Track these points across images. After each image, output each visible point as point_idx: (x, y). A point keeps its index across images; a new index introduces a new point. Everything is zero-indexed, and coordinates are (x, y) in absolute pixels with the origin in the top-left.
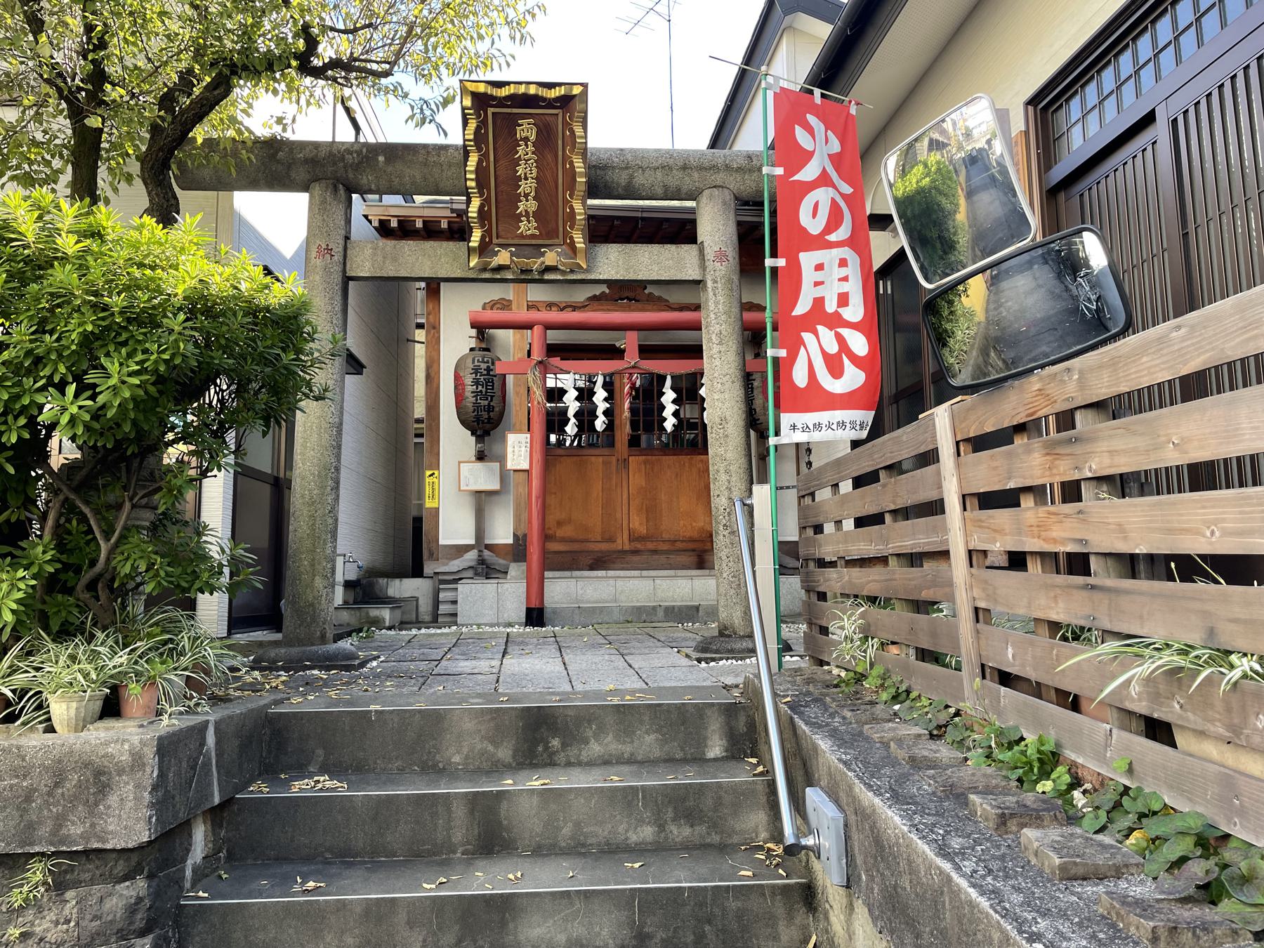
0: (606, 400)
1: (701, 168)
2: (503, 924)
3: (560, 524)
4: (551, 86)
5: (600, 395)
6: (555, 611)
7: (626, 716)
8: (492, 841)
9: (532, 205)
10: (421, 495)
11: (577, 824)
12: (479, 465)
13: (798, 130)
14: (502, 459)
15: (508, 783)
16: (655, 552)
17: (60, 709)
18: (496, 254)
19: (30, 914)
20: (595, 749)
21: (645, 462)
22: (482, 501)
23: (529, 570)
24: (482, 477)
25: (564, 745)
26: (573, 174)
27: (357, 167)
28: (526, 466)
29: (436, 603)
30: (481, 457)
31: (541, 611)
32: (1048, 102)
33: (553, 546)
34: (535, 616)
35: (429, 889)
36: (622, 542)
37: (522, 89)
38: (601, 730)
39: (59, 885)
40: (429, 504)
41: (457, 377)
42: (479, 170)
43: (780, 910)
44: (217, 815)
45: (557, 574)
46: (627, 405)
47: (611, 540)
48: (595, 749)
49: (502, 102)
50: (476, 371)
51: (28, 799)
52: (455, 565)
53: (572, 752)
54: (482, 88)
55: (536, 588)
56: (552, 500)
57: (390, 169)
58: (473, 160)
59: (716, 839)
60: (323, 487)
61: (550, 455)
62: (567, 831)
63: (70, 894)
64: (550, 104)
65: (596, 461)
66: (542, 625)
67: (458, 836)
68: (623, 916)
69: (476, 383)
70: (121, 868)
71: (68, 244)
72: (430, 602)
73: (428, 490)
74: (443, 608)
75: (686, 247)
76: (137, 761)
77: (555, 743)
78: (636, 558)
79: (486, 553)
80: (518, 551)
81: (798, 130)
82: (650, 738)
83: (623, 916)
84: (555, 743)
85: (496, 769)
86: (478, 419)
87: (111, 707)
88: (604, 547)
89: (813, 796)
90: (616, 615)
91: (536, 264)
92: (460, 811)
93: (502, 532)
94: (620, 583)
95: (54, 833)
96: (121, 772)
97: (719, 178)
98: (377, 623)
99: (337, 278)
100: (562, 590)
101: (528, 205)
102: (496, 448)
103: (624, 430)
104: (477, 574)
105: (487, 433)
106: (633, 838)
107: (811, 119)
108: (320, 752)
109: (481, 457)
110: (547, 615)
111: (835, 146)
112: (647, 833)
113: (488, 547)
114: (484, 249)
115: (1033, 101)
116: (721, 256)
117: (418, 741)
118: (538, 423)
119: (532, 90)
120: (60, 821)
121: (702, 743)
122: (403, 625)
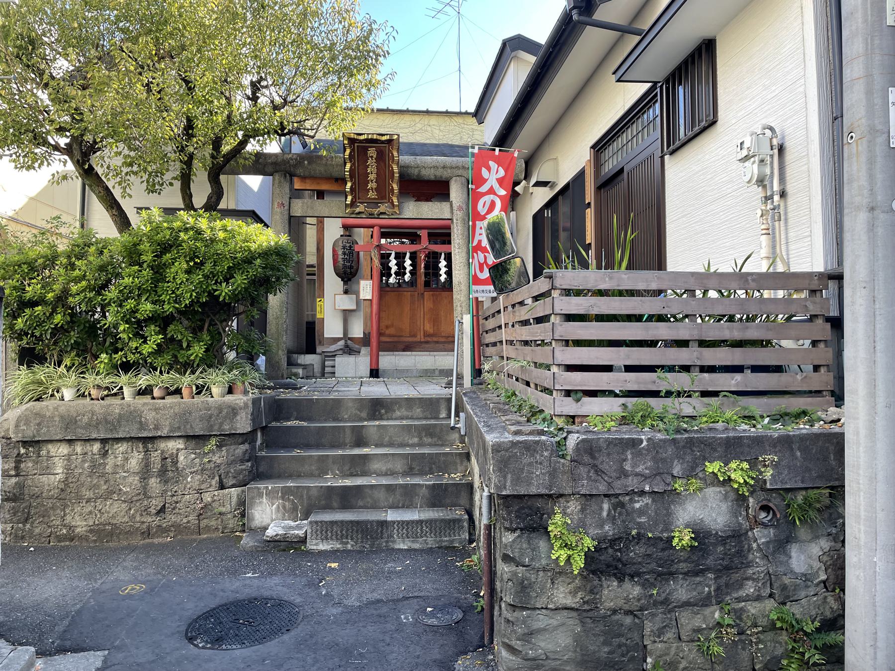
0: (411, 265)
1: (451, 168)
2: (365, 463)
3: (387, 327)
4: (383, 135)
5: (408, 263)
6: (384, 371)
7: (409, 402)
8: (360, 442)
9: (374, 185)
10: (314, 309)
11: (391, 437)
12: (345, 296)
13: (484, 170)
14: (357, 293)
15: (365, 423)
16: (437, 342)
17: (215, 390)
18: (358, 206)
19: (211, 455)
20: (398, 413)
21: (433, 295)
22: (347, 315)
23: (371, 350)
24: (347, 303)
25: (386, 412)
26: (393, 173)
27: (295, 166)
28: (369, 297)
29: (323, 367)
30: (346, 292)
31: (377, 370)
32: (600, 147)
33: (383, 339)
34: (375, 373)
35: (340, 452)
36: (420, 337)
37: (370, 137)
38: (400, 407)
39: (220, 446)
40: (319, 316)
41: (334, 251)
42: (351, 170)
43: (458, 461)
44: (263, 429)
45: (386, 353)
46: (423, 265)
47: (414, 336)
48: (398, 413)
49: (361, 141)
50: (344, 248)
51: (210, 417)
52: (333, 348)
53: (389, 415)
54: (352, 136)
55: (375, 360)
56: (383, 315)
57: (310, 167)
58: (348, 166)
59: (440, 443)
60: (281, 311)
61: (383, 290)
62: (387, 439)
63: (223, 448)
64: (383, 142)
65: (407, 295)
66: (378, 377)
67: (348, 440)
68: (405, 461)
69: (344, 254)
70: (240, 440)
71: (221, 235)
72: (320, 367)
73: (318, 309)
74: (327, 370)
75: (444, 203)
76: (246, 404)
77: (383, 411)
78: (427, 346)
79: (349, 342)
80: (366, 341)
81: (484, 170)
82: (418, 410)
83: (405, 461)
84: (383, 411)
85: (362, 420)
86: (345, 273)
87: (230, 391)
88: (411, 339)
89: (462, 415)
90: (415, 374)
91: (376, 211)
92: (348, 432)
93: (357, 331)
94: (417, 357)
95: (219, 428)
96: (241, 409)
97: (460, 172)
98: (296, 375)
99: (286, 217)
100: (387, 361)
101: (372, 185)
102: (354, 287)
103: (422, 279)
104: (344, 352)
105: (350, 280)
106: (410, 442)
107: (491, 163)
108: (295, 413)
109: (346, 292)
110: (380, 373)
111: (502, 172)
112: (416, 440)
113: (350, 339)
114: (353, 204)
115: (593, 147)
116: (460, 208)
117: (333, 408)
118: (376, 275)
119: (375, 137)
120: (221, 424)
121: (438, 412)
122: (308, 377)
